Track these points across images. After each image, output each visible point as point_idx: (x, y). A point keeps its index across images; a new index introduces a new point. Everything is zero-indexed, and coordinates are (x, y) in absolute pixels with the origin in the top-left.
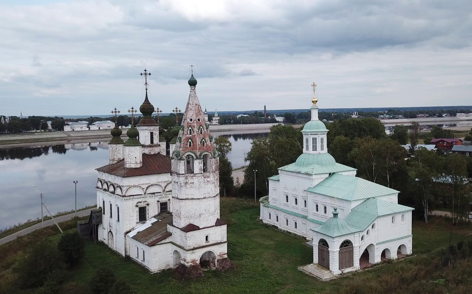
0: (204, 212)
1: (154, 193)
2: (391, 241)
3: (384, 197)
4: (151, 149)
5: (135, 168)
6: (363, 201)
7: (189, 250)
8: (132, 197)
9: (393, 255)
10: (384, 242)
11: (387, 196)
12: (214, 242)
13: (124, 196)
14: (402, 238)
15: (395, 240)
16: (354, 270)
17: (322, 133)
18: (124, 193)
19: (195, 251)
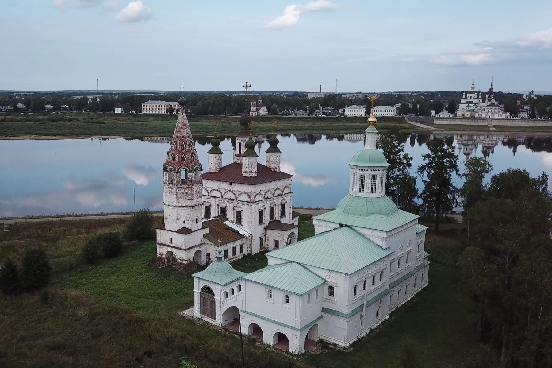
0: (168, 217)
1: (215, 197)
2: (268, 320)
3: (322, 270)
4: (238, 158)
5: (214, 173)
6: (285, 262)
7: (186, 250)
8: (409, 225)
9: (269, 339)
10: (256, 316)
11: (326, 271)
12: (176, 246)
13: (253, 203)
14: (263, 318)
15: (275, 322)
16: (214, 323)
17: (371, 169)
18: (252, 198)
19: (162, 246)
